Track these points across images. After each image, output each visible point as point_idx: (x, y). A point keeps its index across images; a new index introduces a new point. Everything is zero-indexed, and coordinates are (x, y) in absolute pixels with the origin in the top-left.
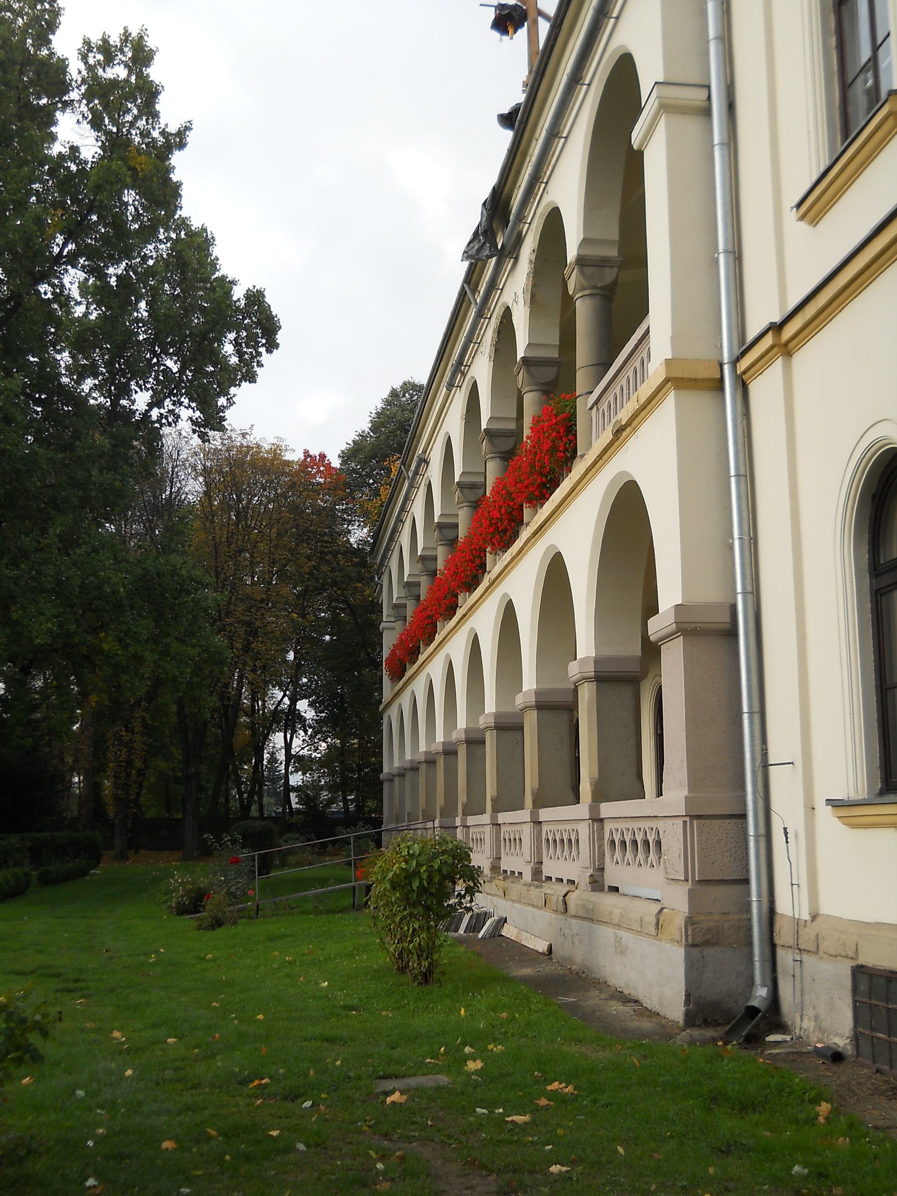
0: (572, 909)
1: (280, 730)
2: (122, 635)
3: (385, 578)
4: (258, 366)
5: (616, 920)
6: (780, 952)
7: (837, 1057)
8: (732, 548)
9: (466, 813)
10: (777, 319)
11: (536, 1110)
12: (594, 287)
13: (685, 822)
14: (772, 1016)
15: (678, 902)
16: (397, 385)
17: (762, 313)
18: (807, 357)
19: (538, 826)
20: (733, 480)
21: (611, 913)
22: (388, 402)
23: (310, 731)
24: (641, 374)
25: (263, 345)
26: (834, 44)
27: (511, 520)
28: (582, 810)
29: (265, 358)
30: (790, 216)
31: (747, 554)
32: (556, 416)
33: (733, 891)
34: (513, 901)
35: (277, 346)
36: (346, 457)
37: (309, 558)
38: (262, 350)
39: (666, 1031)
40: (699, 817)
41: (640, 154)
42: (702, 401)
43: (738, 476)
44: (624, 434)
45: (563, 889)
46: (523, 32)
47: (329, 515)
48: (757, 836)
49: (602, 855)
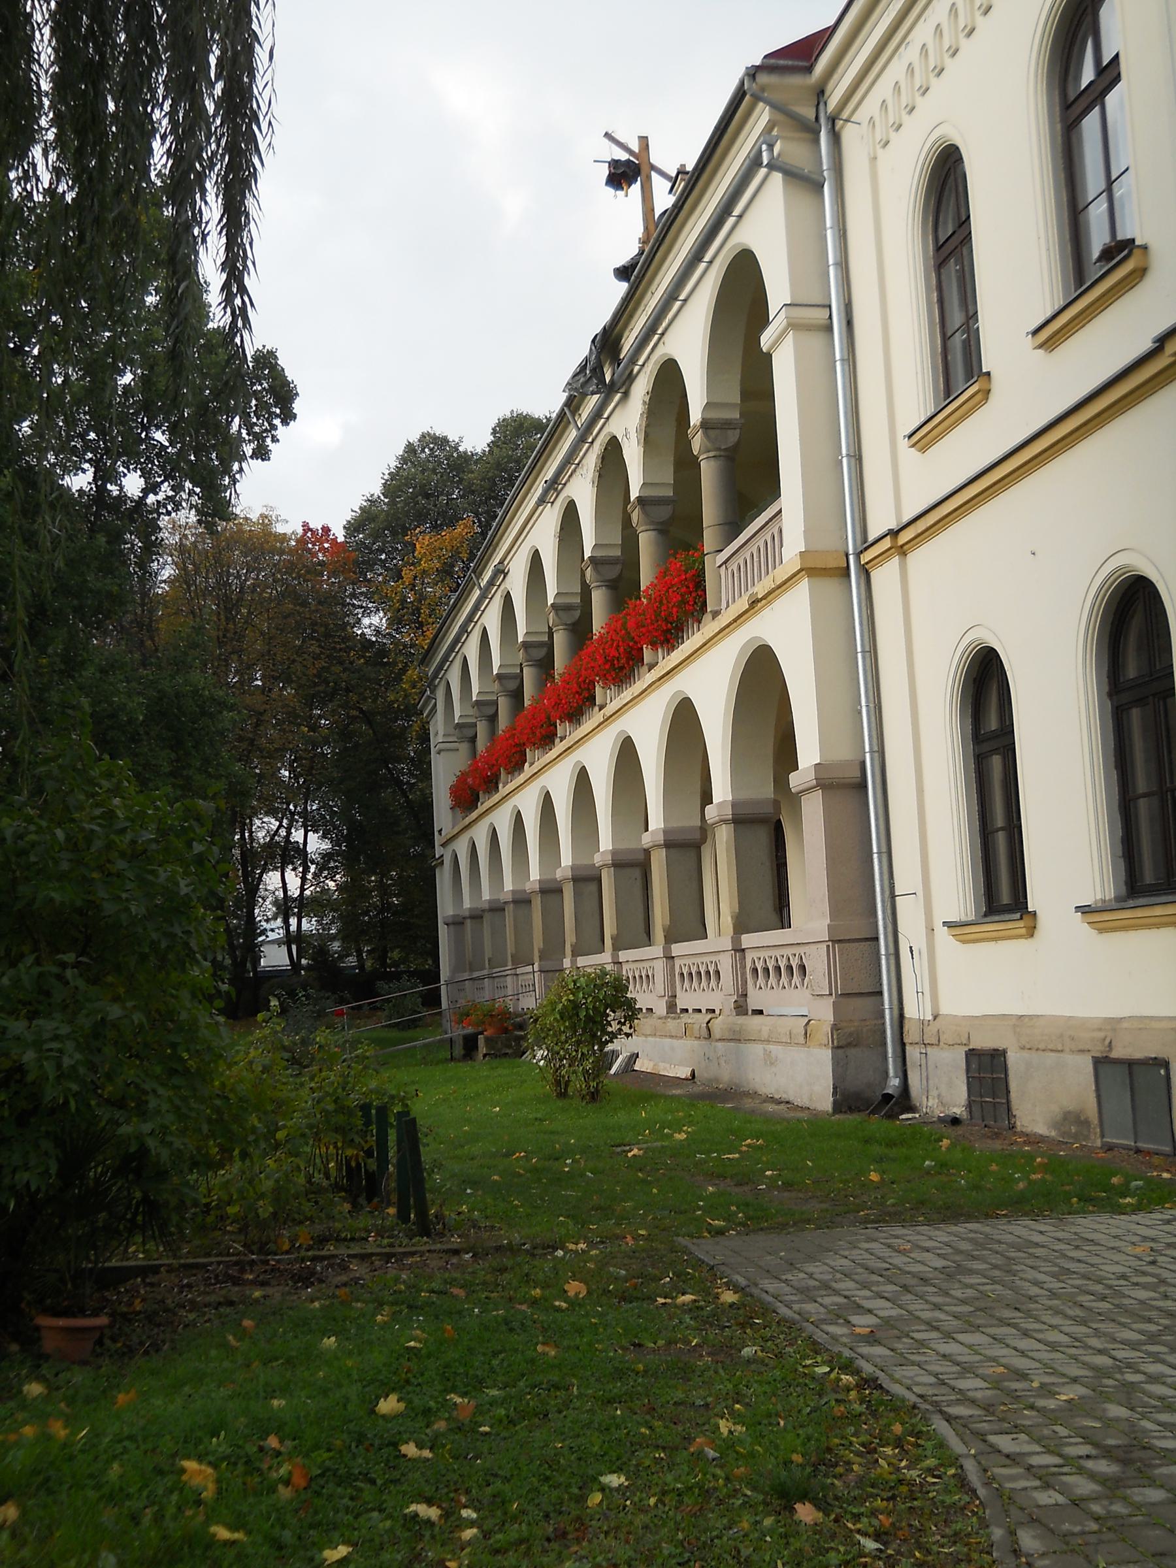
0: (717, 1033)
1: (275, 869)
2: (140, 769)
3: (440, 694)
4: (273, 441)
5: (765, 1035)
6: (908, 1048)
7: (955, 1121)
8: (860, 713)
9: (576, 954)
10: (893, 525)
11: (740, 1152)
12: (719, 449)
13: (828, 946)
14: (903, 1101)
15: (825, 1013)
16: (414, 438)
17: (880, 522)
18: (918, 558)
19: (670, 961)
20: (859, 655)
21: (760, 1031)
22: (404, 460)
23: (313, 868)
24: (777, 560)
25: (277, 416)
26: (936, 300)
27: (629, 659)
28: (656, 950)
29: (281, 431)
30: (903, 444)
31: (873, 719)
32: (686, 572)
33: (869, 1002)
34: (646, 1036)
35: (294, 417)
36: (352, 528)
37: (317, 657)
38: (277, 422)
39: (815, 1117)
40: (839, 941)
41: (769, 356)
42: (831, 586)
43: (863, 652)
44: (759, 605)
45: (704, 1017)
46: (636, 188)
47: (334, 600)
48: (887, 955)
49: (745, 982)
